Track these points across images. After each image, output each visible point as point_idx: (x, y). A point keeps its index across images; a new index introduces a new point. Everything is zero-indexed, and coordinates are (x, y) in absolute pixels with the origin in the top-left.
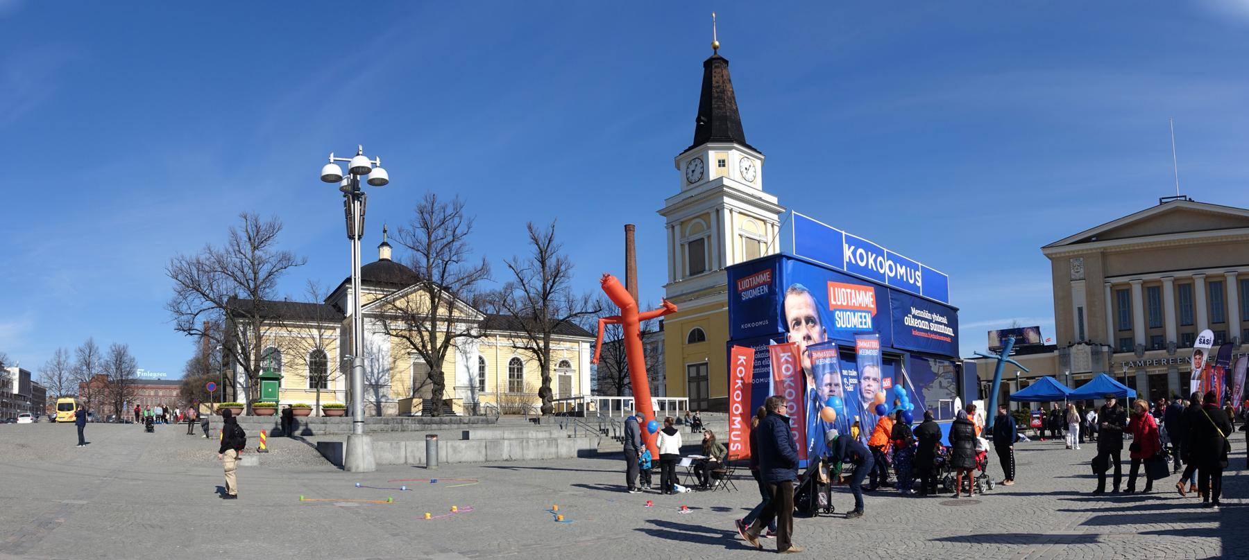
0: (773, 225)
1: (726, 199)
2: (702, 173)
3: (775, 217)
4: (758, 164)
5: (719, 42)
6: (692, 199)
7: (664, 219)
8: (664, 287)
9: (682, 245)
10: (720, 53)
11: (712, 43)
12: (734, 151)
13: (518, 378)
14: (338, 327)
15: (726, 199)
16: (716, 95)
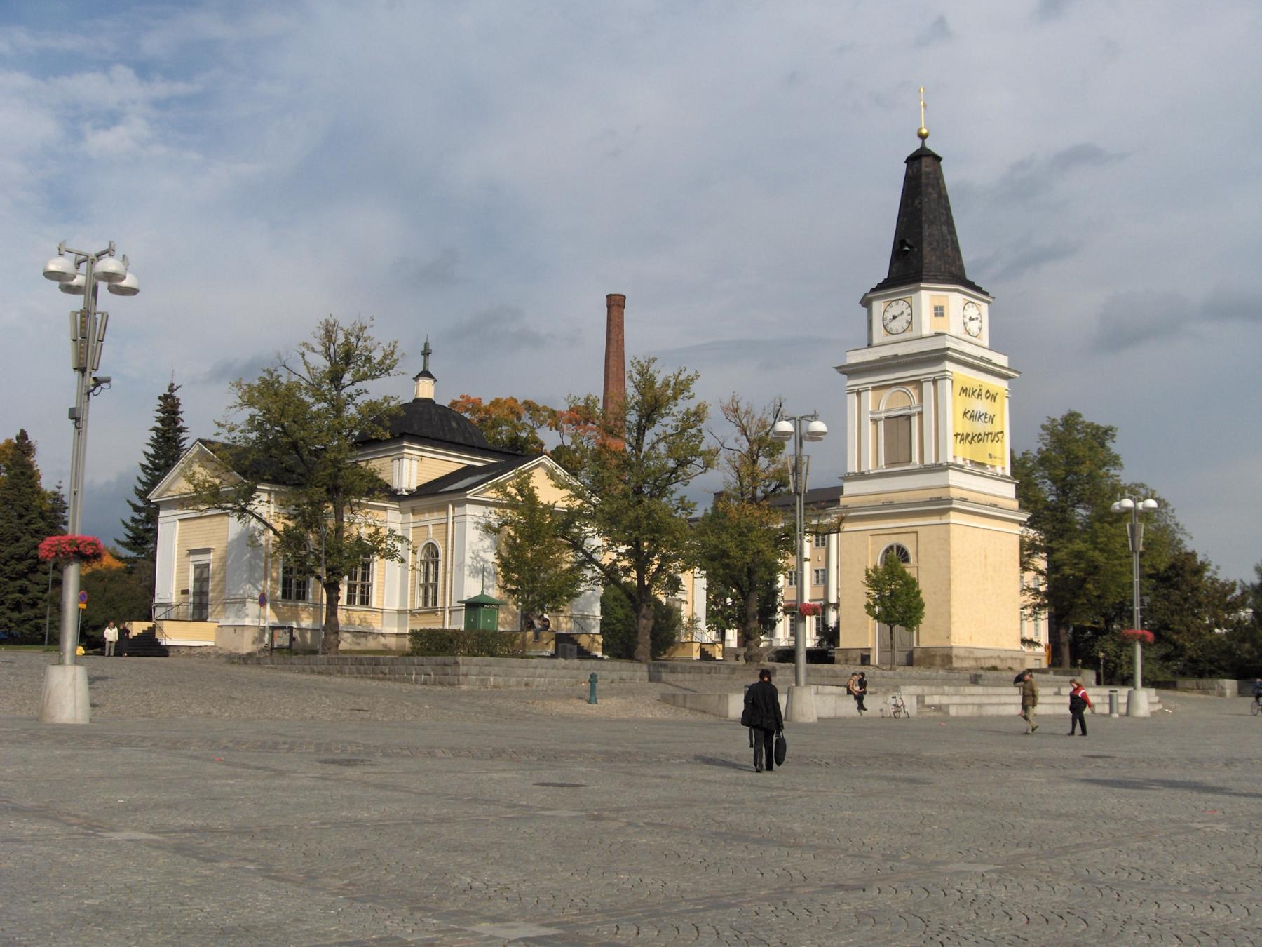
10: (930, 145)
13: (363, 579)
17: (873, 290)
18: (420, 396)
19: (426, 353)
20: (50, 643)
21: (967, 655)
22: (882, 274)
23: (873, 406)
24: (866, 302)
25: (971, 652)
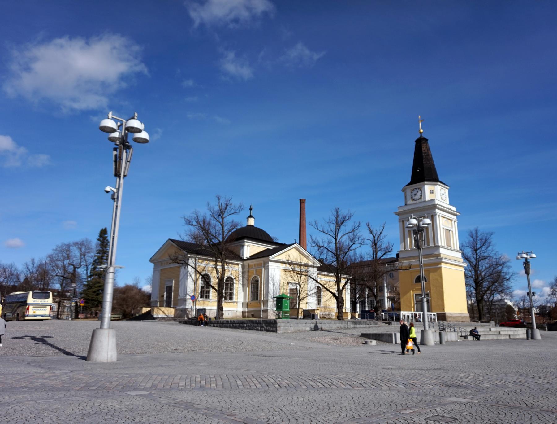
0: (455, 222)
1: (437, 211)
3: (455, 217)
4: (447, 191)
5: (423, 130)
6: (417, 209)
7: (398, 217)
10: (424, 136)
11: (419, 131)
12: (438, 186)
14: (240, 264)
15: (437, 211)
16: (425, 157)
17: (406, 185)
18: (249, 224)
19: (251, 209)
20: (206, 298)
21: (451, 315)
22: (409, 180)
23: (248, 300)
24: (404, 190)
25: (452, 315)
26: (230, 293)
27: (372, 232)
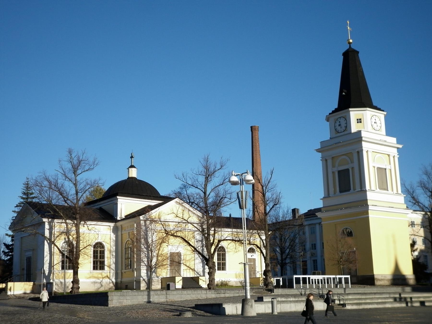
2: (346, 127)
7: (320, 154)
8: (321, 199)
9: (333, 173)
10: (353, 47)
11: (348, 40)
19: (132, 157)
21: (383, 278)
22: (336, 106)
26: (223, 263)
27: (260, 181)
